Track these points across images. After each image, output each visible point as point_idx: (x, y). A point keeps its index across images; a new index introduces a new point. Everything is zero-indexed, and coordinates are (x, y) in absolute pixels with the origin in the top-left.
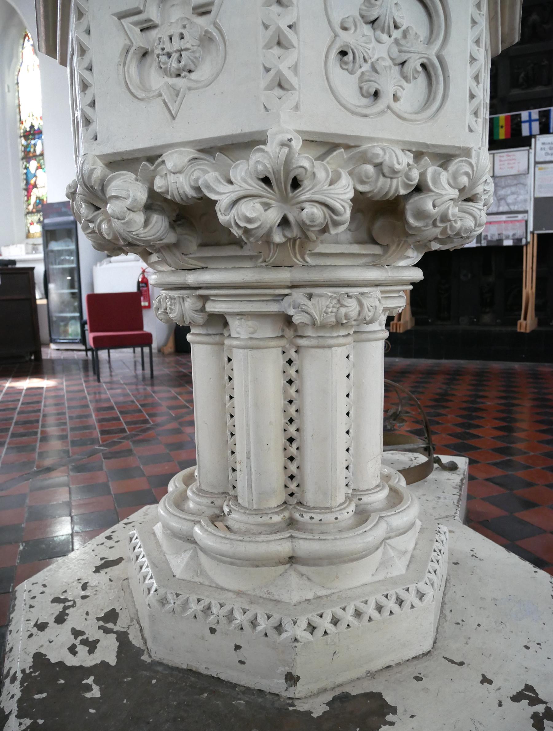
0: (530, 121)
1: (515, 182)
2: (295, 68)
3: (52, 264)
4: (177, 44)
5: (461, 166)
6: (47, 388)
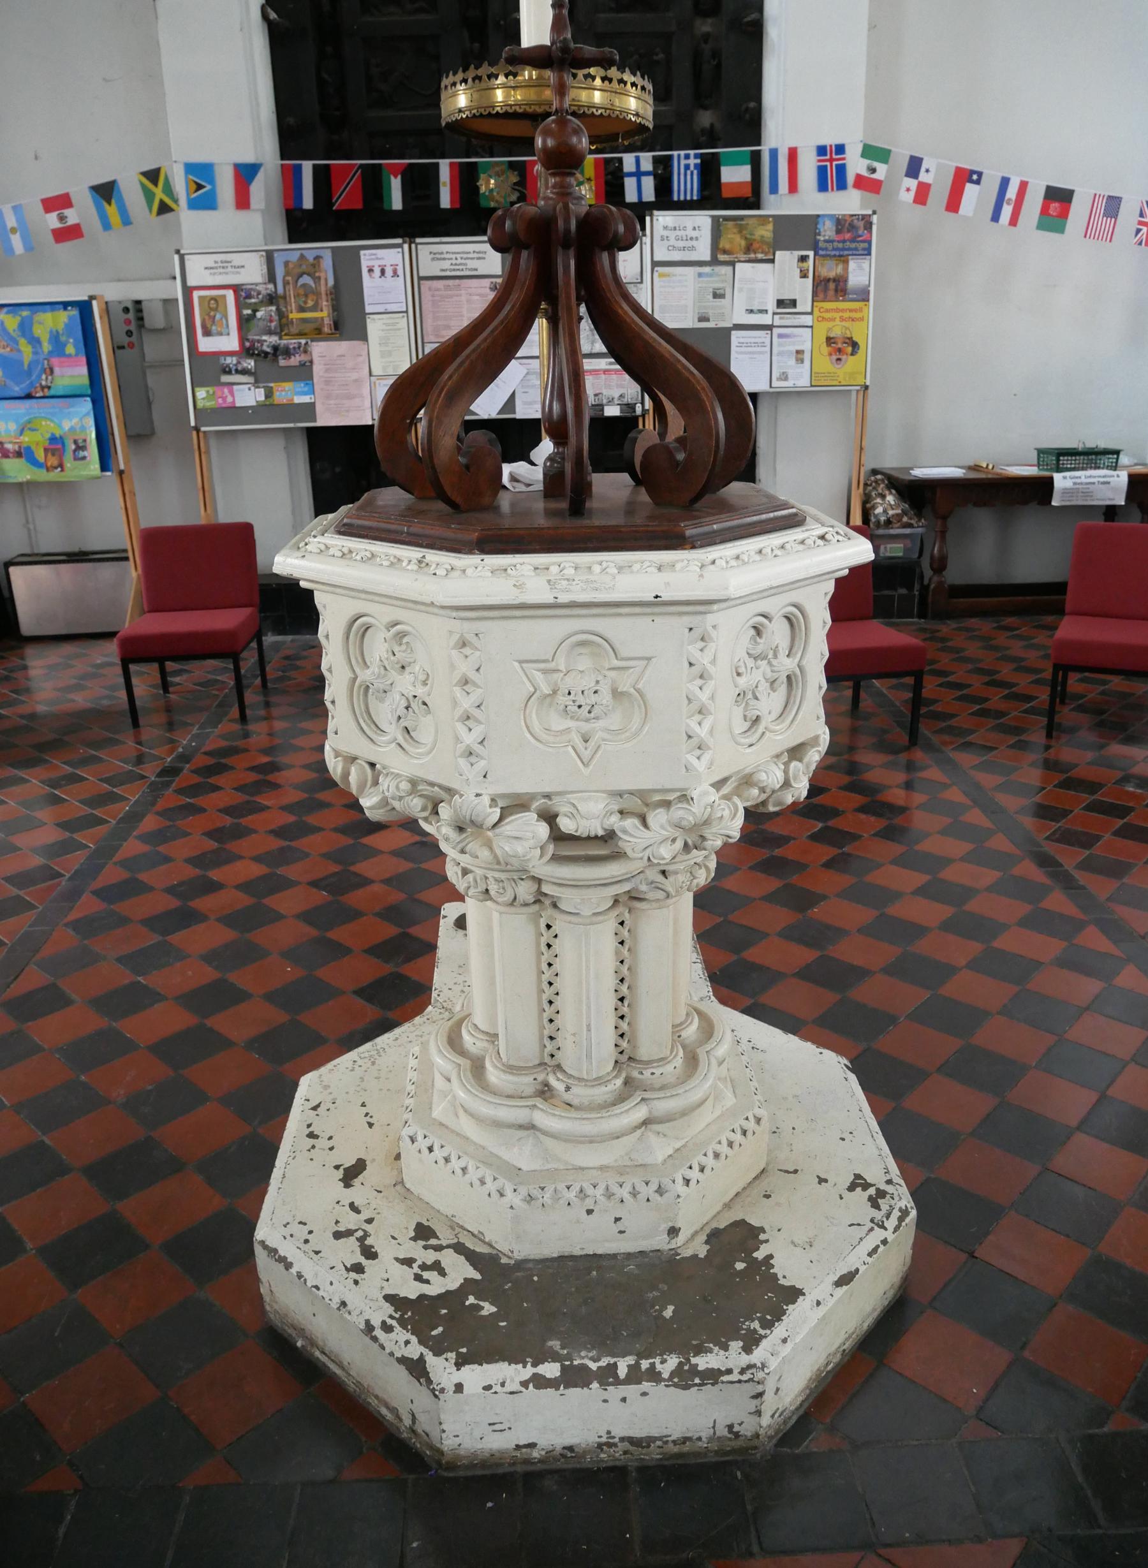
0: (638, 174)
4: (593, 699)
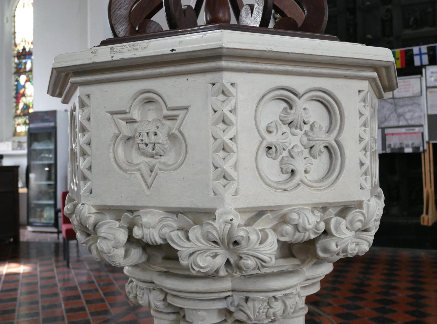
0: (420, 54)
1: (411, 102)
2: (235, 166)
3: (34, 160)
4: (153, 138)
5: (355, 215)
6: (23, 273)
